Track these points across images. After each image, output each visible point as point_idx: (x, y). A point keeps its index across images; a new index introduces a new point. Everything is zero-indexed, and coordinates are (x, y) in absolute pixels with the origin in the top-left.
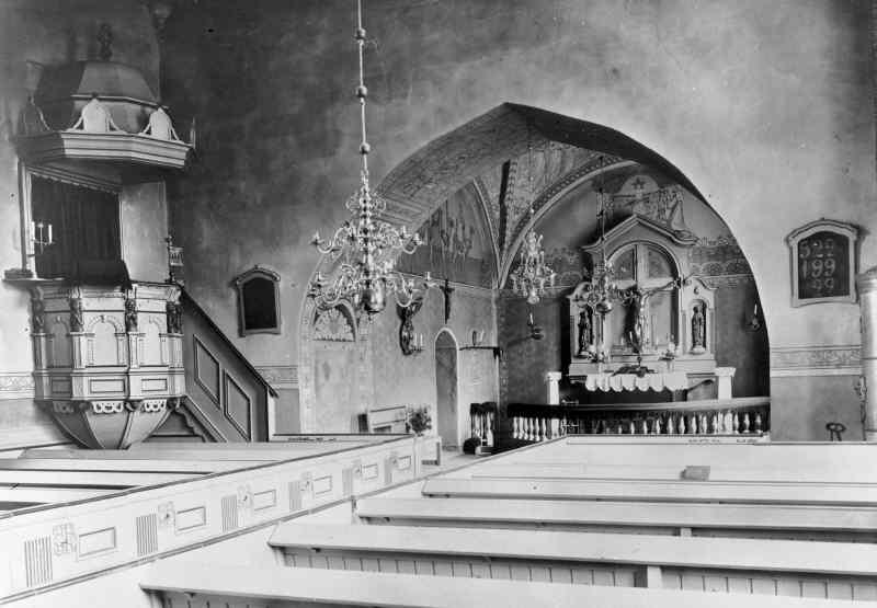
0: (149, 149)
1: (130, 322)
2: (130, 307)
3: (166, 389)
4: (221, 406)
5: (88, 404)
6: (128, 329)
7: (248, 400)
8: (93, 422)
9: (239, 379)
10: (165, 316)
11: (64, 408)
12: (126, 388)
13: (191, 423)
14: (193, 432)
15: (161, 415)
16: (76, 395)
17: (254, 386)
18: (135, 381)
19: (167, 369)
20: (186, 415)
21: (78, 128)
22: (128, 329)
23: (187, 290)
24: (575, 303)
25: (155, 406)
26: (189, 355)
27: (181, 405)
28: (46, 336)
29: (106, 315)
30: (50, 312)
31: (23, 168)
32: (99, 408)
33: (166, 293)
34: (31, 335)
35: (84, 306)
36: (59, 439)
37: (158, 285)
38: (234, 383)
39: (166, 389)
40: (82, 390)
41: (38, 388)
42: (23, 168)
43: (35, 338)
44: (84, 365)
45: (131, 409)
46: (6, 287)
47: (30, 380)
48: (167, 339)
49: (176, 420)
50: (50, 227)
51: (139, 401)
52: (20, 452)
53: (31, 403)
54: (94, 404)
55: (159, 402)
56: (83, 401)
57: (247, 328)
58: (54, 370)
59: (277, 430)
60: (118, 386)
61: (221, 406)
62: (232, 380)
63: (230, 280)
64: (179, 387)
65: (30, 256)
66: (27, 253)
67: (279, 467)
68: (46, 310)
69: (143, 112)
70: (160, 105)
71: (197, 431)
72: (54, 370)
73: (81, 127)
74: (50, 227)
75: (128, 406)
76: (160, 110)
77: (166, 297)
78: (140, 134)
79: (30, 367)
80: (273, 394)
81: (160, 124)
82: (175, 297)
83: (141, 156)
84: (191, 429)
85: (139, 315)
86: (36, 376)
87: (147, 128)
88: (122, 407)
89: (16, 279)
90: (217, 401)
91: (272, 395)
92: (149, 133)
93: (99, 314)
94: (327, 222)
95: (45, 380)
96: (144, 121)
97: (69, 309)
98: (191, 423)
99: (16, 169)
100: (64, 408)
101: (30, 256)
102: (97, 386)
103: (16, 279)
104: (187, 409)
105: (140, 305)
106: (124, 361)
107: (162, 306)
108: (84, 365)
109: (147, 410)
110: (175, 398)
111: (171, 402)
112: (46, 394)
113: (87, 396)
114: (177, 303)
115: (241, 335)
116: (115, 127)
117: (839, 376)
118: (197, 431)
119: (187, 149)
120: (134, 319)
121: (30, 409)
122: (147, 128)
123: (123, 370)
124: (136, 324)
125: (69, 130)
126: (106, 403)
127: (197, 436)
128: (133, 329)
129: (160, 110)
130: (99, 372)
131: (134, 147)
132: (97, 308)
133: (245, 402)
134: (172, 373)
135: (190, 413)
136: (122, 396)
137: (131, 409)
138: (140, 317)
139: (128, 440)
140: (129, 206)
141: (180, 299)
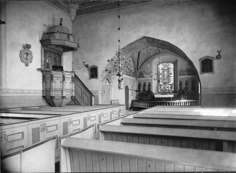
1: (64, 80)
2: (64, 76)
5: (54, 97)
8: (54, 100)
12: (62, 94)
13: (76, 102)
15: (70, 100)
16: (51, 95)
20: (75, 100)
27: (74, 98)
29: (58, 78)
32: (56, 98)
40: (53, 94)
43: (43, 83)
44: (53, 88)
47: (42, 92)
48: (71, 84)
54: (55, 97)
75: (62, 97)
79: (42, 89)
84: (76, 103)
89: (39, 69)
92: (69, 40)
95: (45, 92)
98: (76, 102)
102: (56, 93)
105: (66, 76)
107: (71, 77)
113: (53, 95)
120: (64, 79)
123: (62, 90)
131: (66, 42)
132: (57, 75)
136: (61, 95)
138: (66, 79)
141: (74, 76)
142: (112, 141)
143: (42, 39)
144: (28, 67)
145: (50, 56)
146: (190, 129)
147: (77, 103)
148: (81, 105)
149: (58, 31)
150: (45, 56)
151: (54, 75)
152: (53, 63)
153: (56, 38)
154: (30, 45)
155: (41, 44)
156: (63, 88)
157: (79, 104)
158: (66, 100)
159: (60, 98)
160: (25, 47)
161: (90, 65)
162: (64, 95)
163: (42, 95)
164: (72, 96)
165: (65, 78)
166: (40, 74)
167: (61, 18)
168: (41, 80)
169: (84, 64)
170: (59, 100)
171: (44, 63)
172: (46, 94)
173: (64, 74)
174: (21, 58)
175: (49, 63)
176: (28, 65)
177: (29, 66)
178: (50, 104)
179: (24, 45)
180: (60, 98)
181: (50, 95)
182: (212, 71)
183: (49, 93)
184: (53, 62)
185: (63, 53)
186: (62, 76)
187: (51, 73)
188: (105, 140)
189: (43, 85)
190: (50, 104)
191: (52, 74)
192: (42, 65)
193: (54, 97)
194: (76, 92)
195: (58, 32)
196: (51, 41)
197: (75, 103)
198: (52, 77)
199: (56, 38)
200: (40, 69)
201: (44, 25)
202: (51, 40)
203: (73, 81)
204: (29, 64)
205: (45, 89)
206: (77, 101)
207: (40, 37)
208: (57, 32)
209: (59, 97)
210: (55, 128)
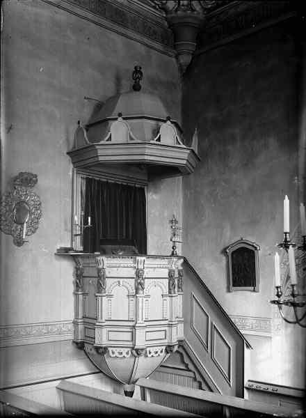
0: (159, 153)
1: (139, 286)
3: (165, 338)
4: (209, 351)
6: (137, 293)
7: (229, 348)
10: (167, 280)
11: (91, 350)
12: (133, 339)
13: (187, 360)
17: (234, 337)
18: (140, 334)
19: (166, 322)
20: (184, 353)
21: (107, 140)
22: (137, 293)
25: (157, 352)
26: (187, 310)
27: (179, 346)
28: (83, 294)
29: (121, 280)
31: (75, 175)
32: (113, 353)
34: (74, 293)
35: (107, 274)
36: (91, 370)
37: (162, 257)
38: (199, 305)
39: (165, 338)
40: (103, 337)
41: (76, 332)
42: (75, 175)
43: (76, 294)
45: (136, 355)
46: (56, 259)
47: (71, 326)
50: (89, 218)
51: (142, 349)
52: (59, 382)
54: (110, 349)
57: (234, 286)
58: (87, 320)
60: (128, 336)
61: (209, 351)
63: (222, 248)
64: (178, 333)
65: (76, 235)
66: (74, 233)
68: (83, 275)
69: (158, 125)
70: (169, 119)
71: (191, 367)
72: (87, 320)
73: (110, 139)
74: (89, 218)
75: (134, 352)
76: (169, 122)
78: (152, 142)
79: (72, 318)
81: (169, 134)
82: (177, 264)
83: (152, 158)
84: (187, 365)
86: (75, 323)
88: (130, 353)
90: (207, 346)
91: (247, 347)
92: (159, 140)
94: (155, 193)
95: (81, 327)
96: (156, 131)
98: (187, 360)
99: (71, 173)
100: (91, 350)
101: (76, 235)
102: (113, 336)
104: (184, 349)
106: (132, 317)
107: (165, 273)
111: (169, 349)
112: (80, 338)
114: (181, 268)
115: (229, 290)
116: (133, 137)
117: (299, 211)
118: (191, 367)
119: (188, 151)
121: (70, 348)
123: (131, 324)
124: (143, 289)
125: (102, 142)
126: (118, 349)
127: (190, 371)
128: (141, 292)
129: (169, 122)
130: (115, 325)
131: (147, 151)
132: (117, 267)
133: (227, 349)
134: (170, 326)
135: (187, 354)
136: (130, 344)
139: (136, 376)
140: (154, 196)
141: (183, 265)
149: (120, 115)
151: (107, 271)
153: (162, 142)
156: (136, 315)
162: (140, 344)
163: (71, 337)
164: (169, 346)
167: (136, 68)
168: (72, 288)
173: (141, 267)
186: (132, 273)
187: (97, 262)
191: (101, 267)
192: (73, 236)
193: (106, 349)
194: (187, 322)
195: (120, 119)
196: (100, 152)
197: (183, 362)
198: (100, 277)
199: (162, 142)
200: (67, 250)
203: (174, 282)
204: (29, 239)
206: (189, 357)
208: (116, 119)
209: (122, 350)
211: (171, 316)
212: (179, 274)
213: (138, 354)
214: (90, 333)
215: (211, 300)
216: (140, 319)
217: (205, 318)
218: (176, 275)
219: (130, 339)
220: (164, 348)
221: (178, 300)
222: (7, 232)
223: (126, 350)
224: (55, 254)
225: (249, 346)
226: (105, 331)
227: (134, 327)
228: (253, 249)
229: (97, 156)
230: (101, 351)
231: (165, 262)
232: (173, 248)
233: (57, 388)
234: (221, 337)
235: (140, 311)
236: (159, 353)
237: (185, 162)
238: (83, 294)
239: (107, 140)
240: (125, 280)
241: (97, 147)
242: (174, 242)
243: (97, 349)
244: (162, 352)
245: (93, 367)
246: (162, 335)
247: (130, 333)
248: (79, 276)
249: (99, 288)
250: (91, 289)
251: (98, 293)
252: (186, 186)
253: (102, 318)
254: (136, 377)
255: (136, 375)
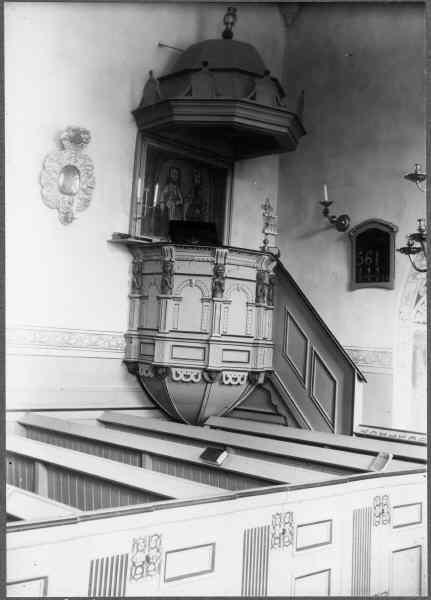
1: (217, 288)
2: (218, 274)
4: (307, 386)
5: (167, 370)
7: (335, 382)
8: (171, 388)
9: (300, 322)
10: (253, 286)
11: (147, 372)
12: (206, 358)
13: (275, 401)
14: (276, 410)
15: (241, 390)
16: (157, 361)
18: (215, 350)
19: (251, 340)
23: (287, 262)
24: (404, 257)
25: (235, 379)
27: (267, 380)
28: (140, 298)
29: (194, 279)
30: (158, 274)
32: (177, 375)
33: (258, 262)
36: (144, 402)
38: (294, 322)
40: (164, 355)
41: (127, 350)
44: (169, 327)
45: (208, 379)
47: (122, 342)
48: (254, 309)
49: (261, 396)
50: (157, 187)
52: (103, 412)
53: (120, 362)
54: (174, 370)
55: (239, 375)
56: (162, 367)
59: (364, 418)
60: (199, 354)
61: (307, 386)
62: (291, 318)
64: (264, 361)
67: (415, 526)
68: (144, 272)
73: (190, 93)
75: (206, 376)
77: (259, 265)
78: (245, 99)
79: (125, 329)
80: (362, 379)
85: (227, 282)
86: (128, 337)
87: (252, 94)
88: (200, 376)
89: (122, 241)
93: (187, 278)
95: (135, 342)
97: (161, 271)
98: (275, 401)
100: (147, 372)
102: (178, 352)
103: (122, 241)
104: (272, 385)
105: (229, 271)
107: (252, 274)
108: (169, 327)
109: (226, 383)
110: (258, 373)
111: (252, 377)
112: (134, 357)
113: (166, 361)
120: (221, 285)
122: (252, 94)
124: (223, 291)
126: (184, 371)
127: (279, 415)
128: (219, 295)
130: (182, 338)
132: (191, 263)
133: (331, 383)
135: (276, 391)
137: (208, 379)
138: (227, 284)
141: (275, 269)
142: (63, 505)
143: (141, 104)
144: (71, 224)
145: (174, 177)
146: (142, 434)
147: (282, 411)
148: (299, 427)
150: (150, 183)
152: (186, 210)
154: (86, 132)
155: (139, 126)
157: (290, 412)
158: (224, 388)
159: (197, 377)
160: (65, 139)
161: (358, 218)
163: (122, 356)
165: (224, 278)
166: (122, 262)
168: (127, 290)
169: (326, 213)
170: (192, 386)
171: (144, 208)
172: (140, 355)
173: (221, 261)
174: (43, 187)
175: (166, 209)
176: (70, 215)
177: (75, 221)
178: (155, 403)
179: (61, 132)
180: (197, 377)
181: (153, 356)
182: (358, 282)
183: (150, 348)
184: (186, 206)
185: (233, 165)
186: (209, 269)
188: (50, 496)
189: (132, 310)
190: (155, 403)
191: (167, 259)
192: (133, 219)
194: (278, 348)
198: (167, 272)
201: (160, 45)
202: (173, 103)
205: (139, 329)
207: (132, 94)
209: (189, 372)
210: (201, 559)
211: (258, 332)
212: (270, 281)
213: (211, 378)
214: (148, 350)
215: (117, 454)
216: (216, 330)
217: (302, 341)
218: (267, 281)
219: (201, 358)
220: (246, 374)
221: (267, 317)
222: (51, 204)
223: (196, 372)
224: (109, 242)
225: (362, 379)
226: (168, 345)
227: (208, 342)
228: (387, 230)
229: (172, 115)
230: (160, 371)
231: (252, 260)
232: (265, 242)
233: (100, 421)
234: (325, 368)
235: (217, 322)
236: (239, 380)
237: (284, 130)
238: (140, 298)
239: (186, 95)
240: (200, 278)
241: (173, 103)
242: (267, 234)
243: (156, 368)
244: (242, 379)
245: (146, 398)
246: (243, 357)
247: (202, 350)
248: (138, 273)
249: (163, 287)
250: (153, 292)
251: (163, 293)
252: (283, 165)
253: (165, 328)
254: (206, 415)
255: (208, 411)
